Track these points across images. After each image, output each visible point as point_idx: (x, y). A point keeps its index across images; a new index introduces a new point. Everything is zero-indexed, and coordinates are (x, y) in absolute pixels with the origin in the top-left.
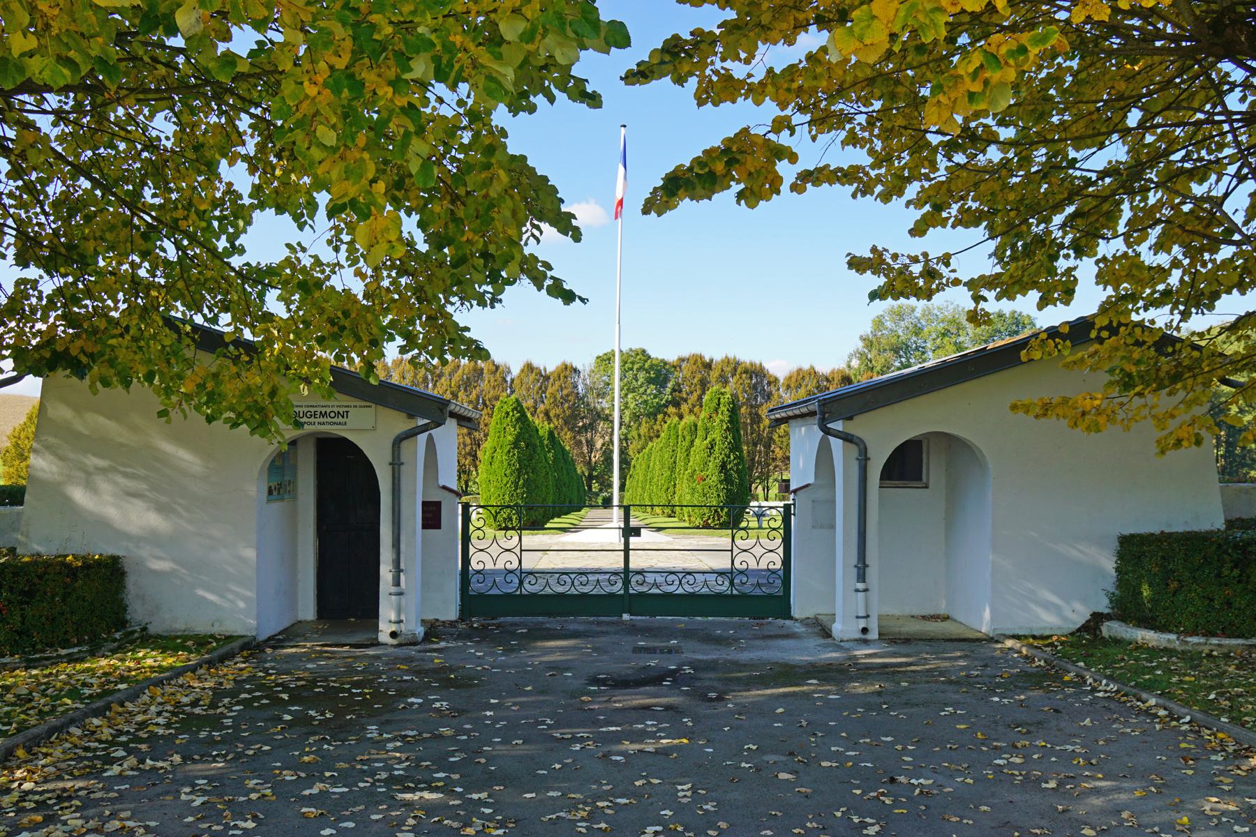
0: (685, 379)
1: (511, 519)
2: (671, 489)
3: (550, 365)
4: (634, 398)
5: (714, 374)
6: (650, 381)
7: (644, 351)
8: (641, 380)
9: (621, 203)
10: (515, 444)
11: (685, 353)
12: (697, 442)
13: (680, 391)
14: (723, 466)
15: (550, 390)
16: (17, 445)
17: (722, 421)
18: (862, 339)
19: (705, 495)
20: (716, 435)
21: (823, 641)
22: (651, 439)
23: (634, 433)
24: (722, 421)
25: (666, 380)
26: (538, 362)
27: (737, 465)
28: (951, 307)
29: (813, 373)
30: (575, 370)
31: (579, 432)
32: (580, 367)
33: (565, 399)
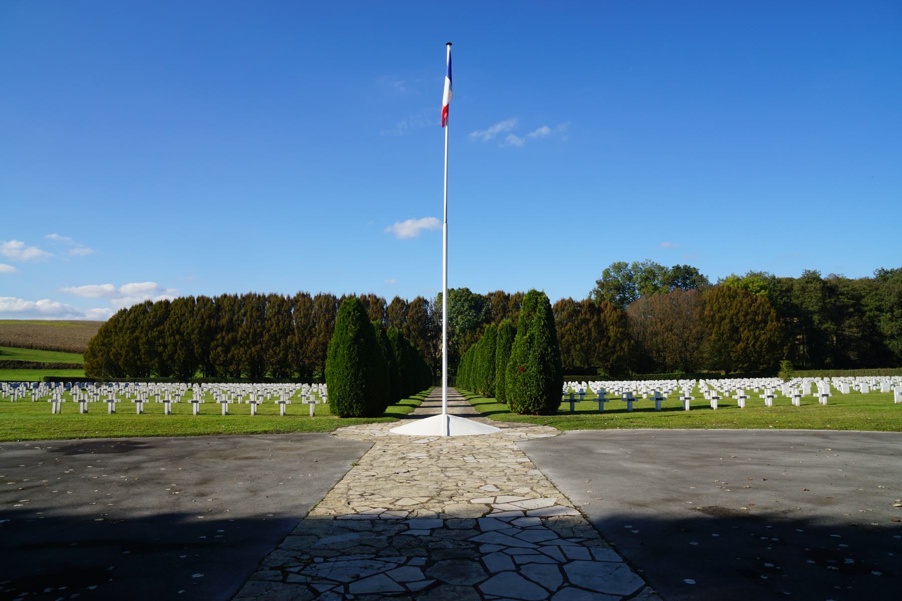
0: (493, 305)
1: (352, 407)
2: (490, 377)
3: (410, 298)
4: (462, 318)
5: (511, 303)
6: (471, 308)
7: (468, 290)
8: (466, 307)
9: (447, 109)
10: (355, 340)
11: (493, 291)
12: (518, 337)
13: (490, 313)
14: (542, 358)
15: (410, 314)
16: (91, 349)
17: (539, 318)
18: (597, 282)
19: (525, 384)
20: (535, 330)
21: (544, 431)
22: (473, 343)
23: (462, 340)
24: (539, 318)
25: (481, 307)
26: (403, 297)
27: (553, 357)
28: (649, 263)
29: (571, 301)
30: (426, 302)
31: (429, 340)
32: (429, 300)
33: (419, 319)
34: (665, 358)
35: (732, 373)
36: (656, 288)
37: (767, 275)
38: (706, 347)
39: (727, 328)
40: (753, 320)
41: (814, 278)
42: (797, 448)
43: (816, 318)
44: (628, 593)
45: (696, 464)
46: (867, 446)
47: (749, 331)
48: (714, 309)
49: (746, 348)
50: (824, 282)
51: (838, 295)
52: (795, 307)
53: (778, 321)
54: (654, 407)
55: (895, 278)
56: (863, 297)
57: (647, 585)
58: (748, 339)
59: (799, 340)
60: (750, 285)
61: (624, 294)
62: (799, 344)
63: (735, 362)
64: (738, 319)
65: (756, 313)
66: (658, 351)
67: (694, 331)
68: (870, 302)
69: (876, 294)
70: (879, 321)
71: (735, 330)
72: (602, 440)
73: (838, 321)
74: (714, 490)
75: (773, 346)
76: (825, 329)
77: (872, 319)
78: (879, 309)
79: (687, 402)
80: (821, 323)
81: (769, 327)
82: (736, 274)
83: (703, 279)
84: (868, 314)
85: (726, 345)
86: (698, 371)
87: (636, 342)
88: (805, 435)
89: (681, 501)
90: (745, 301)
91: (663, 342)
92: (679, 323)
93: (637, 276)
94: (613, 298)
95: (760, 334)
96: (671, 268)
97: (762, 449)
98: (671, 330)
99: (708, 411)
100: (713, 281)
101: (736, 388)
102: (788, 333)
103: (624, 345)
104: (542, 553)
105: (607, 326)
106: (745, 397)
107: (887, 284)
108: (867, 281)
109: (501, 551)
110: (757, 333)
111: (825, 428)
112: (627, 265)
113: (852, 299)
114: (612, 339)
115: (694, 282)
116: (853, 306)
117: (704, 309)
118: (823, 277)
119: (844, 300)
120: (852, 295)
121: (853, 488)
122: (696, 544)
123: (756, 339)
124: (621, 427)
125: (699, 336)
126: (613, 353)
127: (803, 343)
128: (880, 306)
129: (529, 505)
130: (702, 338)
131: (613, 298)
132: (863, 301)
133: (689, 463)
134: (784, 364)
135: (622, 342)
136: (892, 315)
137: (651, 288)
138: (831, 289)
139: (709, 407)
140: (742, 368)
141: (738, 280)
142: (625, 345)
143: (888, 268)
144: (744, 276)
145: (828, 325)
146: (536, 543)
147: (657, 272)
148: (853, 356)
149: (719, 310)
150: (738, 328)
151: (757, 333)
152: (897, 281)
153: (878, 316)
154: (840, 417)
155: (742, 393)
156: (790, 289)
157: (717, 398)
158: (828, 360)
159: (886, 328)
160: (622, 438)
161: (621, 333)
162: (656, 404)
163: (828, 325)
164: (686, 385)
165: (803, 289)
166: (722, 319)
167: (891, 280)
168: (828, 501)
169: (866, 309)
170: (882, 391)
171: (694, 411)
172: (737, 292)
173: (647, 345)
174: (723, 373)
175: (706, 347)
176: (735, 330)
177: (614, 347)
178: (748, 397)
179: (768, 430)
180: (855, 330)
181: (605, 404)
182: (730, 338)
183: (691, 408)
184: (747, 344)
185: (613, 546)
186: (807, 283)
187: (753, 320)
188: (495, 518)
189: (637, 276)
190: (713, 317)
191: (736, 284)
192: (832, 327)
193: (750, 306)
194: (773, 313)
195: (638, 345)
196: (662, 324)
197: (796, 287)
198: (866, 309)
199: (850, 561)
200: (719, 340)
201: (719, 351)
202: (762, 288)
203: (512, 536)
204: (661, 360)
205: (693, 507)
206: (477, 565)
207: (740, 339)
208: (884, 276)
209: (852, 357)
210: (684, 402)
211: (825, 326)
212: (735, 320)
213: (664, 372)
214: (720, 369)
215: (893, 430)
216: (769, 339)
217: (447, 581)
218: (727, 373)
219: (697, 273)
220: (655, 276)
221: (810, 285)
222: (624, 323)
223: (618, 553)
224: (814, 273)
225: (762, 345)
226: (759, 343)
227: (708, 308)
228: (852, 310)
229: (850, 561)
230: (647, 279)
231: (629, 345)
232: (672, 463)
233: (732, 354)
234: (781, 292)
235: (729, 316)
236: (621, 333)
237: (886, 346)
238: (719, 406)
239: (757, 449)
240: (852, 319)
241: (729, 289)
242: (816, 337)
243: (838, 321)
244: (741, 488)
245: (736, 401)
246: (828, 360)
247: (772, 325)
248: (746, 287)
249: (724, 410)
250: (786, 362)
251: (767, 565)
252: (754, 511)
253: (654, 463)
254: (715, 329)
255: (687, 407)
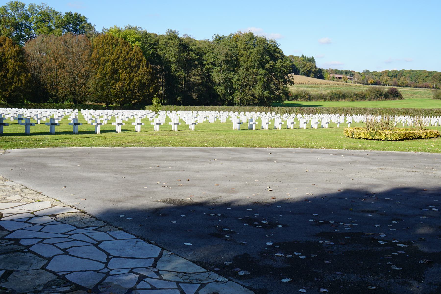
18: (110, 28)
28: (45, 7)
34: (57, 91)
35: (110, 105)
36: (50, 30)
37: (140, 30)
38: (92, 83)
39: (109, 69)
40: (129, 65)
41: (174, 37)
42: (194, 159)
43: (173, 67)
44: (156, 256)
45: (136, 172)
46: (235, 157)
47: (126, 73)
48: (100, 53)
49: (123, 86)
50: (181, 40)
51: (189, 51)
52: (159, 57)
53: (148, 67)
55: (225, 42)
56: (205, 54)
57: (163, 249)
58: (125, 79)
59: (160, 82)
60: (128, 36)
61: (21, 32)
62: (160, 86)
63: (113, 97)
64: (118, 63)
65: (132, 60)
67: (83, 70)
68: (208, 58)
69: (213, 53)
70: (213, 72)
71: (115, 71)
72: (45, 157)
73: (187, 71)
74: (161, 189)
75: (142, 86)
76: (179, 76)
77: (208, 71)
78: (213, 64)
79: (99, 127)
81: (140, 71)
82: (118, 26)
83: (90, 27)
84: (206, 66)
86: (84, 103)
87: (33, 75)
89: (144, 197)
90: (124, 49)
91: (57, 77)
92: (71, 62)
93: (33, 18)
94: (10, 35)
95: (134, 76)
96: (64, 14)
97: (173, 161)
98: (64, 68)
100: (99, 29)
101: (121, 116)
102: (153, 77)
103: (21, 78)
104: (75, 240)
105: (5, 59)
106: (141, 124)
107: (219, 46)
108: (206, 42)
109: (39, 242)
110: (132, 75)
111: (204, 146)
112: (24, 5)
113: (198, 55)
114: (10, 71)
115: (83, 28)
116: (198, 60)
117: (91, 52)
118: (180, 36)
119: (192, 55)
120: (198, 52)
121: (242, 182)
122: (175, 222)
123: (131, 79)
124: (56, 146)
125: (87, 74)
126: (11, 84)
127: (162, 85)
128: (214, 61)
129: (35, 207)
130: (89, 76)
131: (10, 35)
132: (205, 57)
133: (130, 171)
134: (155, 100)
135: (19, 74)
136: (221, 69)
137: (45, 29)
138: (184, 46)
139: (114, 131)
140: (119, 102)
141: (119, 31)
142: (22, 77)
143: (221, 35)
144: (124, 28)
145: (181, 73)
146: (64, 234)
147: (51, 15)
148: (195, 96)
149: (104, 54)
150: (117, 70)
151: (132, 75)
152: (226, 44)
153: (212, 69)
154: (210, 139)
156: (156, 43)
157: (121, 124)
158: (179, 99)
159: (216, 78)
160: (64, 155)
161: (19, 67)
162: (51, 128)
163: (181, 73)
164: (72, 114)
165: (166, 44)
166: (106, 62)
167: (222, 43)
168: (233, 190)
169: (205, 63)
170: (221, 121)
172: (117, 41)
173: (42, 78)
174: (104, 105)
175: (92, 83)
176: (115, 71)
177: (12, 78)
178: (143, 124)
179: (168, 147)
180: (197, 77)
181: (31, 127)
182: (112, 78)
183: (102, 132)
184: (124, 83)
185: (122, 229)
186: (169, 39)
187: (129, 65)
188: (11, 220)
189: (33, 18)
190: (99, 59)
191: (117, 35)
192: (184, 74)
193: (128, 53)
194: (144, 61)
195: (35, 79)
196: (56, 62)
197: (161, 42)
198: (205, 63)
199: (264, 222)
201: (102, 87)
202: (137, 40)
203: (39, 231)
205: (154, 200)
206: (28, 255)
208: (219, 40)
209: (194, 97)
210: (96, 127)
211: (178, 74)
212: (116, 64)
214: (101, 102)
215: (243, 146)
217: (15, 269)
218: (107, 105)
219: (86, 21)
220: (49, 19)
221: (171, 41)
222: (22, 58)
223: (129, 233)
224: (174, 32)
225: (135, 85)
226: (132, 83)
227: (95, 52)
228: (197, 63)
229: (264, 222)
230: (42, 20)
231: (25, 78)
232: (117, 172)
233: (112, 91)
234: (151, 44)
235: (111, 59)
236: (19, 67)
237: (215, 90)
238: (122, 130)
239: (170, 161)
240: (196, 70)
241: (113, 38)
242: (171, 81)
243: (187, 71)
244: (177, 186)
245: (134, 127)
246: (179, 99)
247: (143, 70)
248: (125, 38)
249: (125, 133)
250: (157, 98)
251: (224, 229)
252: (196, 200)
253: (104, 172)
254: (100, 69)
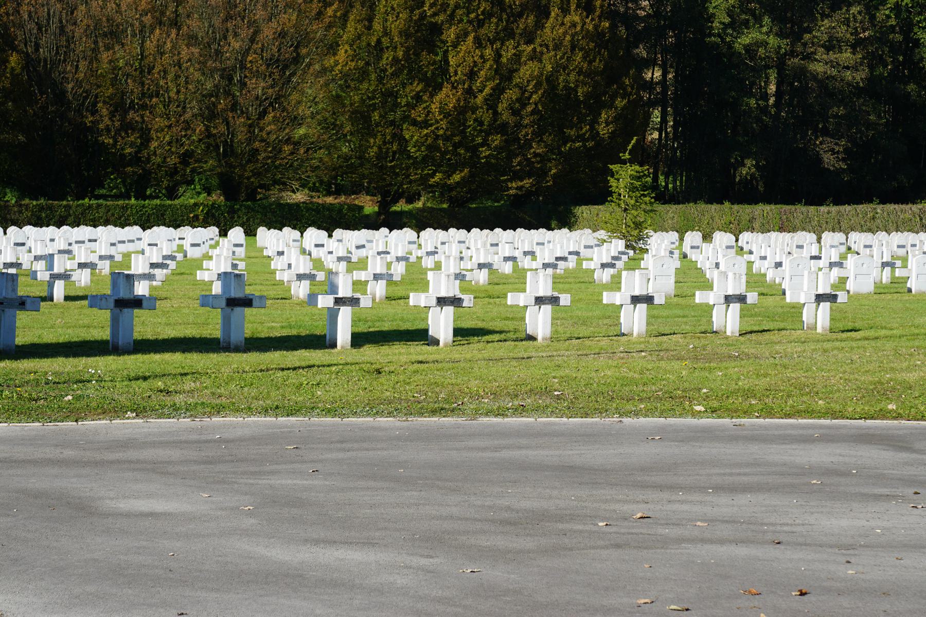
34: (146, 139)
35: (401, 206)
38: (310, 95)
39: (396, 25)
42: (831, 485)
45: (528, 543)
47: (478, 43)
49: (463, 110)
54: (217, 333)
58: (472, 75)
62: (653, 104)
66: (119, 107)
67: (267, 32)
75: (560, 108)
76: (750, 50)
79: (345, 316)
80: (736, 25)
85: (391, 94)
86: (274, 194)
87: (29, 62)
88: (828, 438)
91: (145, 70)
95: (517, 56)
97: (719, 489)
98: (175, 23)
99: (416, 350)
106: (554, 300)
110: (507, 55)
124: (140, 412)
127: (662, 102)
130: (297, 60)
133: (500, 542)
134: (623, 177)
139: (421, 336)
140: (445, 190)
148: (830, 155)
150: (436, 29)
155: (541, 285)
157: (455, 302)
158: (748, 168)
160: (175, 454)
171: (369, 352)
173: (75, 76)
174: (370, 206)
175: (310, 95)
179: (690, 421)
180: (846, 56)
182: (408, 67)
183: (358, 340)
184: (469, 92)
192: (773, 41)
200: (364, 74)
201: (361, 117)
204: (128, 145)
207: (443, 69)
209: (828, 160)
210: (333, 315)
211: (746, 39)
213: (141, 196)
214: (356, 189)
216: (551, 80)
218: (384, 206)
225: (523, 101)
226: (511, 94)
240: (839, 15)
246: (748, 168)
249: (475, 349)
254: (352, 27)
255: (343, 336)
